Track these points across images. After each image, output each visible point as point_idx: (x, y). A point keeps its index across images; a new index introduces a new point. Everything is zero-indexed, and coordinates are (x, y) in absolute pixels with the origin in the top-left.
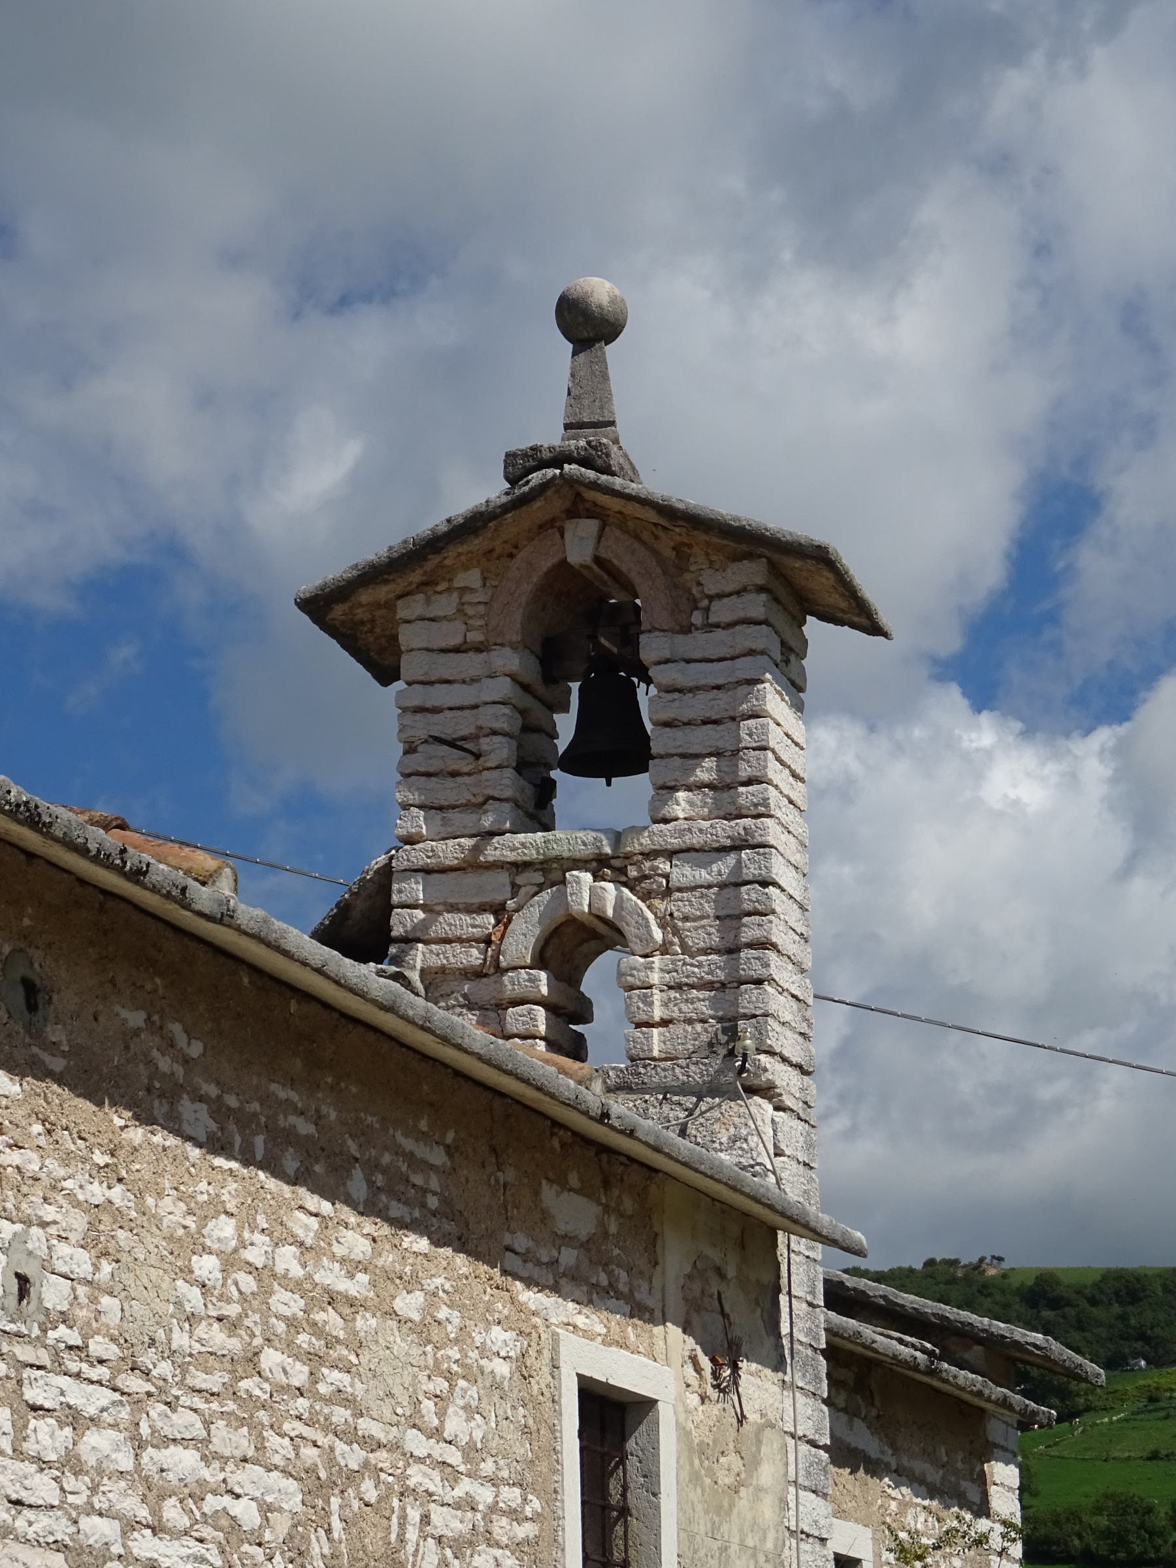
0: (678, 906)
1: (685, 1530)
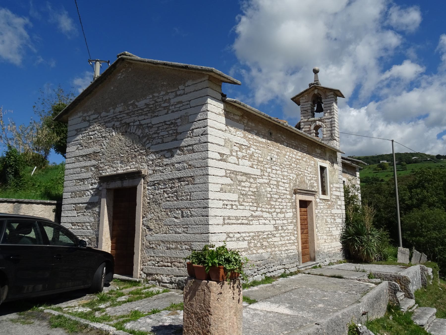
0: (326, 124)
1: (329, 178)
